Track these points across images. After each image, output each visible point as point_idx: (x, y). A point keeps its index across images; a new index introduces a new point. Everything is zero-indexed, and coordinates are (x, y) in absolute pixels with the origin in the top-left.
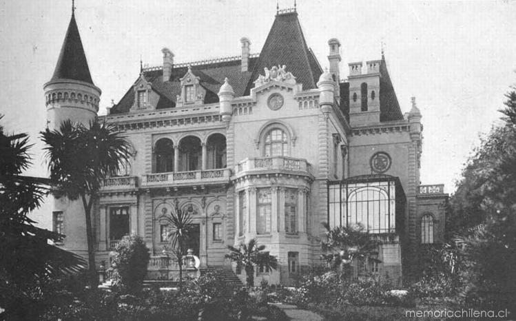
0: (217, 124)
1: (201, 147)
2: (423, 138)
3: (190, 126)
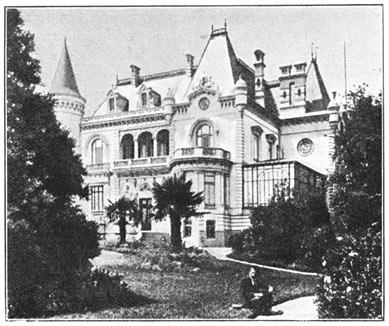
0: (163, 122)
1: (152, 141)
2: (67, 133)
3: (144, 124)
